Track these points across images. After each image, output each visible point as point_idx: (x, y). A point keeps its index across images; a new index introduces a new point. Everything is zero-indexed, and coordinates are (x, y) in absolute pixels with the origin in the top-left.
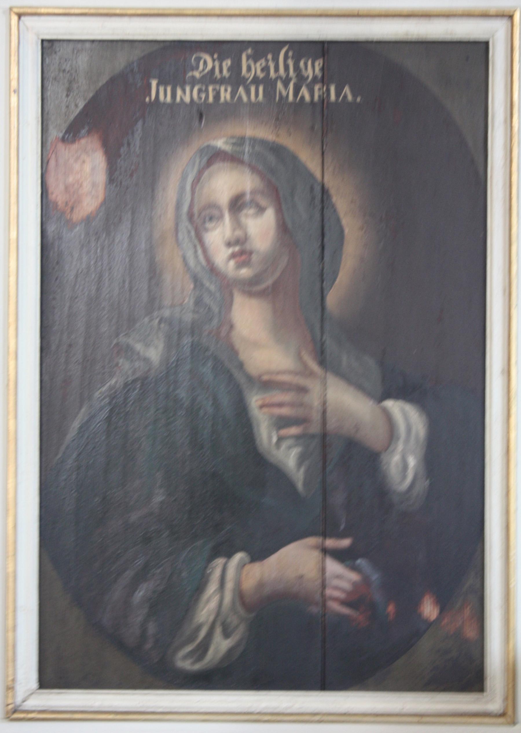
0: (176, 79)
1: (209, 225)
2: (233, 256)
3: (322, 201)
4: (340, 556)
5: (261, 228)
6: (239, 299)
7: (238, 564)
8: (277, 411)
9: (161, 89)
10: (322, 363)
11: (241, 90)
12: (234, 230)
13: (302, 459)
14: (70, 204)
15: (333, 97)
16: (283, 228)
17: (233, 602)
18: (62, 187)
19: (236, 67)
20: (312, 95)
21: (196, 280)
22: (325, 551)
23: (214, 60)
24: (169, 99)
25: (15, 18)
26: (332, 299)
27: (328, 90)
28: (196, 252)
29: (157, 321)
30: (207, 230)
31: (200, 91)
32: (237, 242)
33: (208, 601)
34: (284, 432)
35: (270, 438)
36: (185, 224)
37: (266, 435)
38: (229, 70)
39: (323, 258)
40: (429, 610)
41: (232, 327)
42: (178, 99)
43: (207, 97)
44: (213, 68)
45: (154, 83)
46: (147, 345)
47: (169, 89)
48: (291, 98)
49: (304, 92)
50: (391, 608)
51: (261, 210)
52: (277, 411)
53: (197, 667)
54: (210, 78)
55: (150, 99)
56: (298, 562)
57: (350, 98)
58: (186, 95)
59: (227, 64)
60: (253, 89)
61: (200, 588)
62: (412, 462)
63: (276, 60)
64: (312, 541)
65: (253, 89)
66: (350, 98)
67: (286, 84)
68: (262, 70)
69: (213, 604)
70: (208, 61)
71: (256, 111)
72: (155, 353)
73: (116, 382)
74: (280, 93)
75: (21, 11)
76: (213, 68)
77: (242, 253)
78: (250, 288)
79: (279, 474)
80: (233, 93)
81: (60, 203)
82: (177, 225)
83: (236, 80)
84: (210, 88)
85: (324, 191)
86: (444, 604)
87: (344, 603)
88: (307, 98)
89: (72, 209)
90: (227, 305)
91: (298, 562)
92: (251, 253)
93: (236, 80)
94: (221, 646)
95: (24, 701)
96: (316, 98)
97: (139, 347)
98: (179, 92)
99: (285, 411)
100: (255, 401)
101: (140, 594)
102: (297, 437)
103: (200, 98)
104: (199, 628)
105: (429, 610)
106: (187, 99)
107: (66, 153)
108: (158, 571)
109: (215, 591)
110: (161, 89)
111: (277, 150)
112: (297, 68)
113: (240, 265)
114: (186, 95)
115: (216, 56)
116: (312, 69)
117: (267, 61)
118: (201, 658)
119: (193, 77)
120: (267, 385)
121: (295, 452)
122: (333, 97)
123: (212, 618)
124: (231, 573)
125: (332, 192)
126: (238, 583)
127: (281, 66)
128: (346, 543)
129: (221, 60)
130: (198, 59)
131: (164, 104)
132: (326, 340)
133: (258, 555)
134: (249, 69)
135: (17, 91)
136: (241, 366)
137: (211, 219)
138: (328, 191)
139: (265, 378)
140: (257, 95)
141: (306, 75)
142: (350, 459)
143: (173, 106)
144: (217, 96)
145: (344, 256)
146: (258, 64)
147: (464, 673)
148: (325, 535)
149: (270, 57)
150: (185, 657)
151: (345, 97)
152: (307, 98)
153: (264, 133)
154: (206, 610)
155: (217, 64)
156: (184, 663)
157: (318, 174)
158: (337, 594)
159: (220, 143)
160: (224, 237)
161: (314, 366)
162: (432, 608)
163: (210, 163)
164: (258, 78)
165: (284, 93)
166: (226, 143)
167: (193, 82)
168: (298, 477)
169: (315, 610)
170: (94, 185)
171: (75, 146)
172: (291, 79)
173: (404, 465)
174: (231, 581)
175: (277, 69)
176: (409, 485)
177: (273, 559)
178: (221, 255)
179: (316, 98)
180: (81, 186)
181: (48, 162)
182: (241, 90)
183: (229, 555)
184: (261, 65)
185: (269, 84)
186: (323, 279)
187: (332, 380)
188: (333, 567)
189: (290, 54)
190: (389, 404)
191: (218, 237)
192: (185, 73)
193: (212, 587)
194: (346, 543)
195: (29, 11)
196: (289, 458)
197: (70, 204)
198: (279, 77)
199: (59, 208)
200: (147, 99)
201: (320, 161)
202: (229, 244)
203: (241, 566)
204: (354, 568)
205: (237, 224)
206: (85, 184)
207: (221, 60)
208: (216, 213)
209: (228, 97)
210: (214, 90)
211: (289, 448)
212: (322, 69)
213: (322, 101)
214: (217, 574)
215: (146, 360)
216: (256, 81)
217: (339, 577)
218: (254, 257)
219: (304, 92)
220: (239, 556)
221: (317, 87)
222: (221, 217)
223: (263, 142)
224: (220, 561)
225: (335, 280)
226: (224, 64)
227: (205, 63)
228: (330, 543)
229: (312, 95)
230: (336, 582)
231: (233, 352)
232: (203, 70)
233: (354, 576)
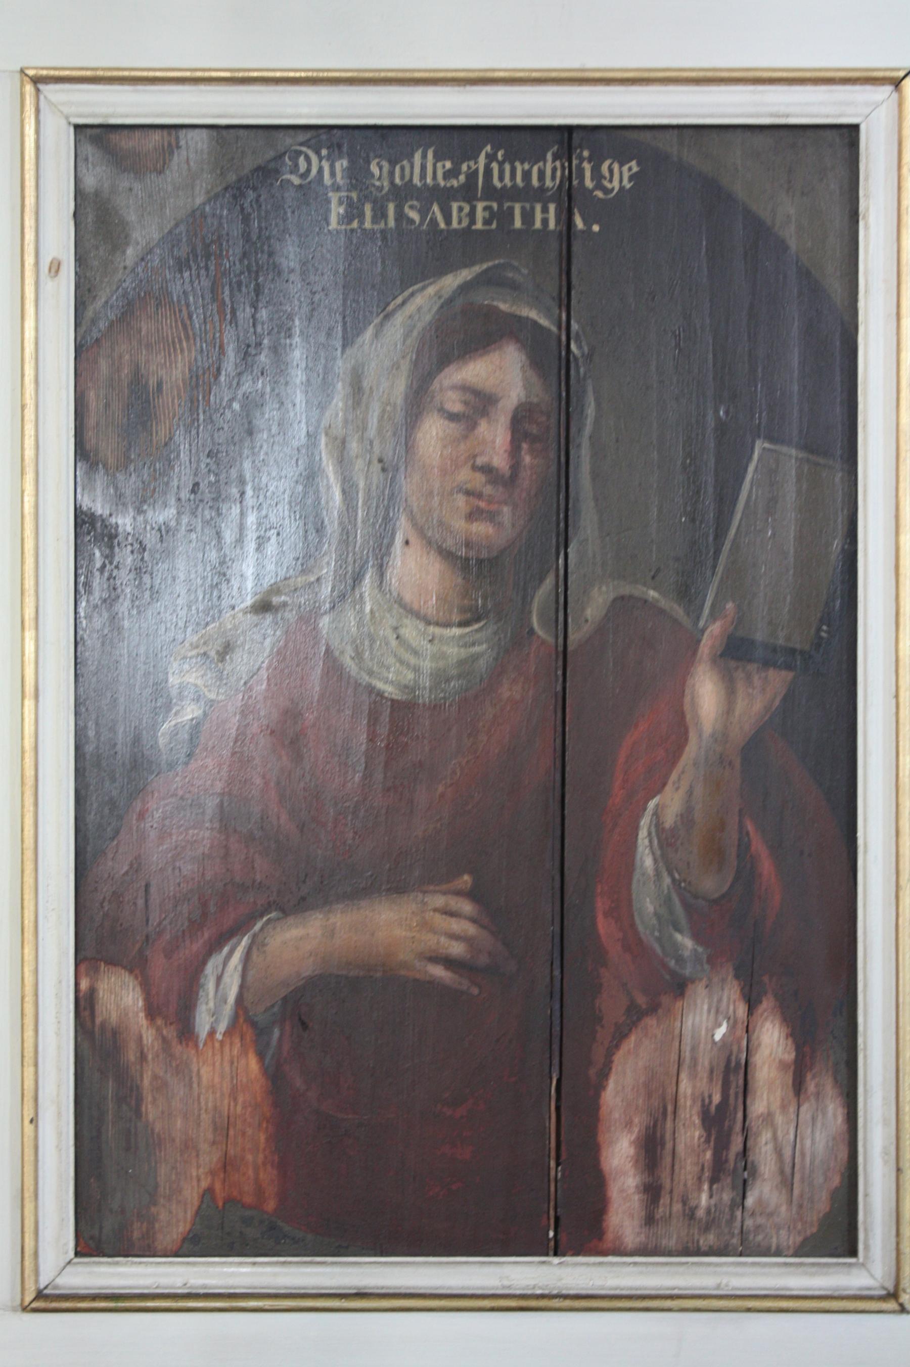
23: (321, 159)
38: (631, 179)
44: (320, 170)
59: (444, 166)
115: (324, 152)
146: (625, 168)
155: (326, 165)
182: (435, 208)
184: (630, 169)
227: (308, 159)
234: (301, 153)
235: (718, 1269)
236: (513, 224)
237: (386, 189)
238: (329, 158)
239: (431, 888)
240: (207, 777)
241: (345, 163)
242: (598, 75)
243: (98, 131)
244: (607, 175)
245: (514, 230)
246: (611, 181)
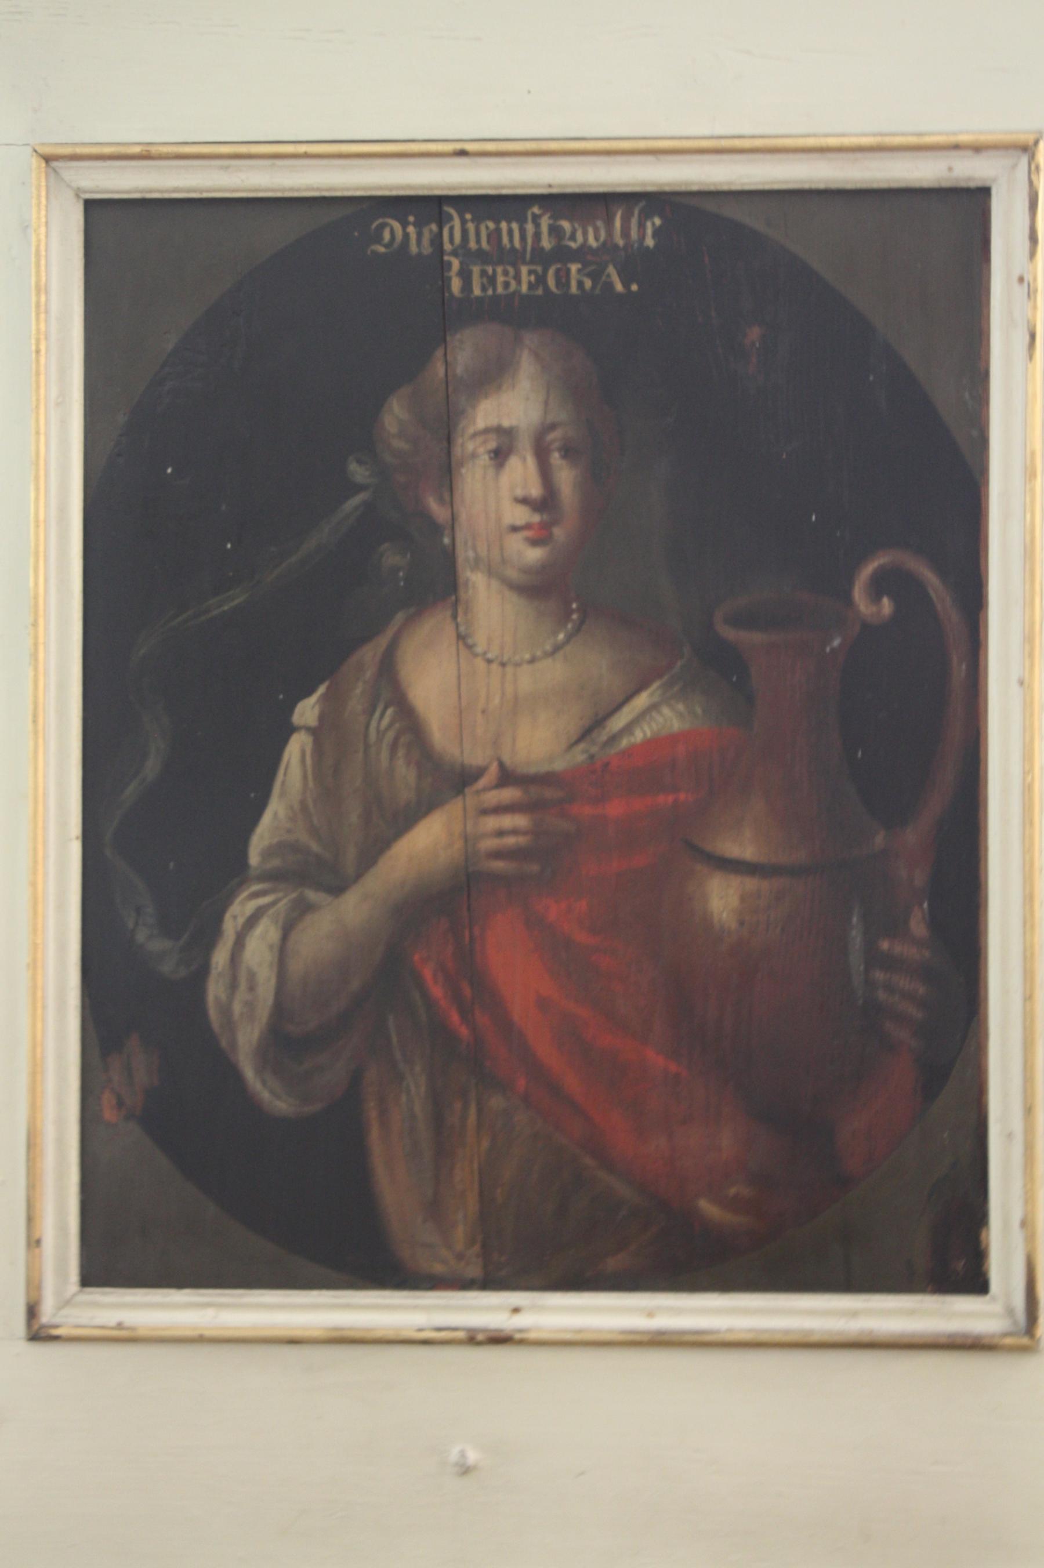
38: (656, 233)
44: (406, 236)
57: (619, 287)
66: (619, 287)
130: (383, 226)
155: (411, 229)
210: (483, 273)
226: (649, 224)
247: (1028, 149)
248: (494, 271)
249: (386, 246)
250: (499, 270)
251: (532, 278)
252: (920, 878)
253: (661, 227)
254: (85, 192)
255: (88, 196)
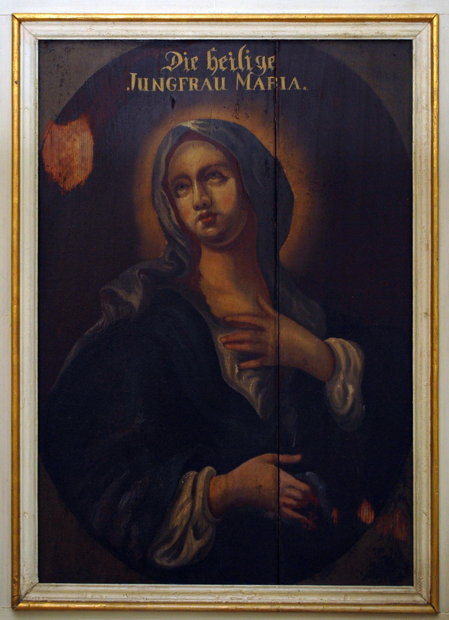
0: (152, 70)
1: (181, 192)
2: (201, 218)
3: (275, 172)
4: (291, 469)
5: (224, 193)
6: (206, 253)
7: (207, 476)
8: (239, 347)
9: (140, 81)
10: (276, 307)
11: (207, 80)
12: (201, 196)
13: (259, 387)
14: (63, 175)
15: (283, 87)
16: (242, 192)
17: (203, 508)
18: (56, 161)
19: (202, 62)
20: (266, 87)
21: (169, 236)
22: (280, 465)
23: (183, 57)
24: (146, 88)
25: (16, 22)
26: (284, 253)
27: (280, 80)
28: (170, 213)
29: (137, 271)
30: (178, 196)
31: (172, 82)
32: (205, 206)
33: (182, 507)
34: (244, 365)
35: (233, 369)
36: (160, 190)
37: (229, 366)
38: (196, 65)
39: (276, 219)
40: (366, 514)
41: (200, 276)
42: (154, 88)
43: (178, 87)
44: (184, 62)
45: (134, 75)
46: (129, 291)
47: (146, 80)
48: (248, 88)
49: (259, 82)
50: (335, 514)
51: (224, 179)
52: (239, 347)
53: (173, 564)
54: (180, 71)
55: (130, 88)
56: (256, 474)
57: (298, 87)
58: (161, 85)
59: (195, 60)
60: (216, 80)
61: (176, 495)
62: (351, 389)
63: (235, 56)
64: (268, 456)
65: (216, 80)
66: (298, 87)
67: (244, 77)
68: (224, 65)
69: (186, 510)
70: (179, 58)
71: (217, 98)
72: (135, 300)
73: (103, 323)
74: (240, 83)
75: (21, 17)
76: (184, 62)
77: (208, 215)
78: (216, 244)
79: (240, 398)
80: (200, 84)
81: (54, 174)
82: (153, 191)
83: (202, 72)
84: (181, 79)
85: (277, 163)
86: (378, 510)
87: (294, 509)
88: (262, 88)
89: (65, 179)
90: (196, 259)
91: (256, 474)
92: (216, 215)
93: (202, 72)
94: (193, 545)
95: (27, 593)
96: (269, 88)
97: (121, 293)
98: (155, 83)
99: (245, 347)
100: (220, 339)
101: (124, 502)
102: (255, 369)
103: (172, 87)
104: (175, 530)
105: (366, 514)
106: (162, 89)
107: (59, 133)
108: (140, 482)
109: (187, 499)
110: (140, 81)
111: (236, 129)
112: (253, 63)
113: (207, 225)
114: (161, 85)
115: (185, 53)
116: (266, 64)
117: (228, 57)
118: (176, 556)
119: (167, 70)
120: (230, 325)
121: (253, 382)
122: (283, 87)
123: (185, 522)
124: (201, 484)
125: (283, 164)
126: (207, 492)
127: (241, 61)
128: (297, 458)
129: (190, 57)
130: (171, 55)
131: (142, 92)
132: (279, 288)
133: (223, 468)
134: (213, 64)
135: (18, 83)
136: (208, 309)
137: (182, 186)
138: (279, 163)
139: (229, 319)
140: (220, 85)
141: (260, 68)
142: (299, 386)
143: (150, 94)
144: (186, 86)
145: (293, 217)
146: (220, 60)
147: (395, 567)
148: (279, 453)
149: (230, 54)
150: (163, 555)
151: (294, 86)
152: (262, 88)
153: (225, 116)
154: (180, 515)
155: (186, 59)
156: (162, 560)
157: (271, 150)
158: (290, 501)
159: (189, 124)
160: (193, 202)
161: (271, 311)
162: (367, 522)
163: (181, 141)
164: (221, 70)
165: (243, 83)
166: (194, 124)
167: (167, 74)
168: (257, 404)
169: (271, 515)
170: (83, 159)
171: (68, 127)
172: (248, 72)
173: (345, 392)
174: (202, 490)
175: (236, 64)
176: (348, 409)
177: (236, 471)
178: (191, 217)
179: (269, 88)
180: (72, 160)
181: (44, 141)
182: (207, 80)
183: (199, 469)
184: (223, 60)
185: (230, 76)
186: (277, 239)
187: (284, 320)
188: (286, 478)
189: (248, 51)
190: (332, 341)
191: (188, 201)
192: (160, 66)
193: (186, 496)
194: (297, 458)
195: (28, 17)
196: (249, 386)
197: (63, 175)
198: (239, 70)
199: (53, 178)
200: (128, 89)
201: (273, 139)
202: (197, 208)
203: (209, 478)
204: (303, 480)
205: (204, 191)
206: (75, 159)
207: (190, 57)
208: (186, 181)
209: (196, 86)
210: (184, 81)
211: (249, 378)
212: (274, 64)
213: (274, 90)
214: (190, 483)
215: (130, 305)
216: (219, 74)
217: (291, 487)
218: (219, 218)
219: (259, 82)
220: (207, 469)
221: (270, 78)
222: (192, 185)
223: (225, 123)
224: (192, 474)
225: (287, 236)
226: (192, 59)
227: (177, 59)
228: (283, 458)
229: (266, 87)
230: (289, 492)
231: (202, 299)
232: (175, 65)
233: (303, 486)
234: (174, 55)
235: (418, 519)
236: (209, 89)
237: (264, 71)
238: (188, 56)
239: (222, 369)
240: (137, 306)
241: (196, 58)
242: (394, 17)
243: (132, 47)
244: (259, 63)
245: (261, 91)
246: (261, 65)
247: (430, 21)
248: (189, 80)
249: (172, 67)
250: (191, 80)
251: (184, 83)
252: (106, 288)
253: (198, 61)
254: (39, 36)
255: (40, 38)
